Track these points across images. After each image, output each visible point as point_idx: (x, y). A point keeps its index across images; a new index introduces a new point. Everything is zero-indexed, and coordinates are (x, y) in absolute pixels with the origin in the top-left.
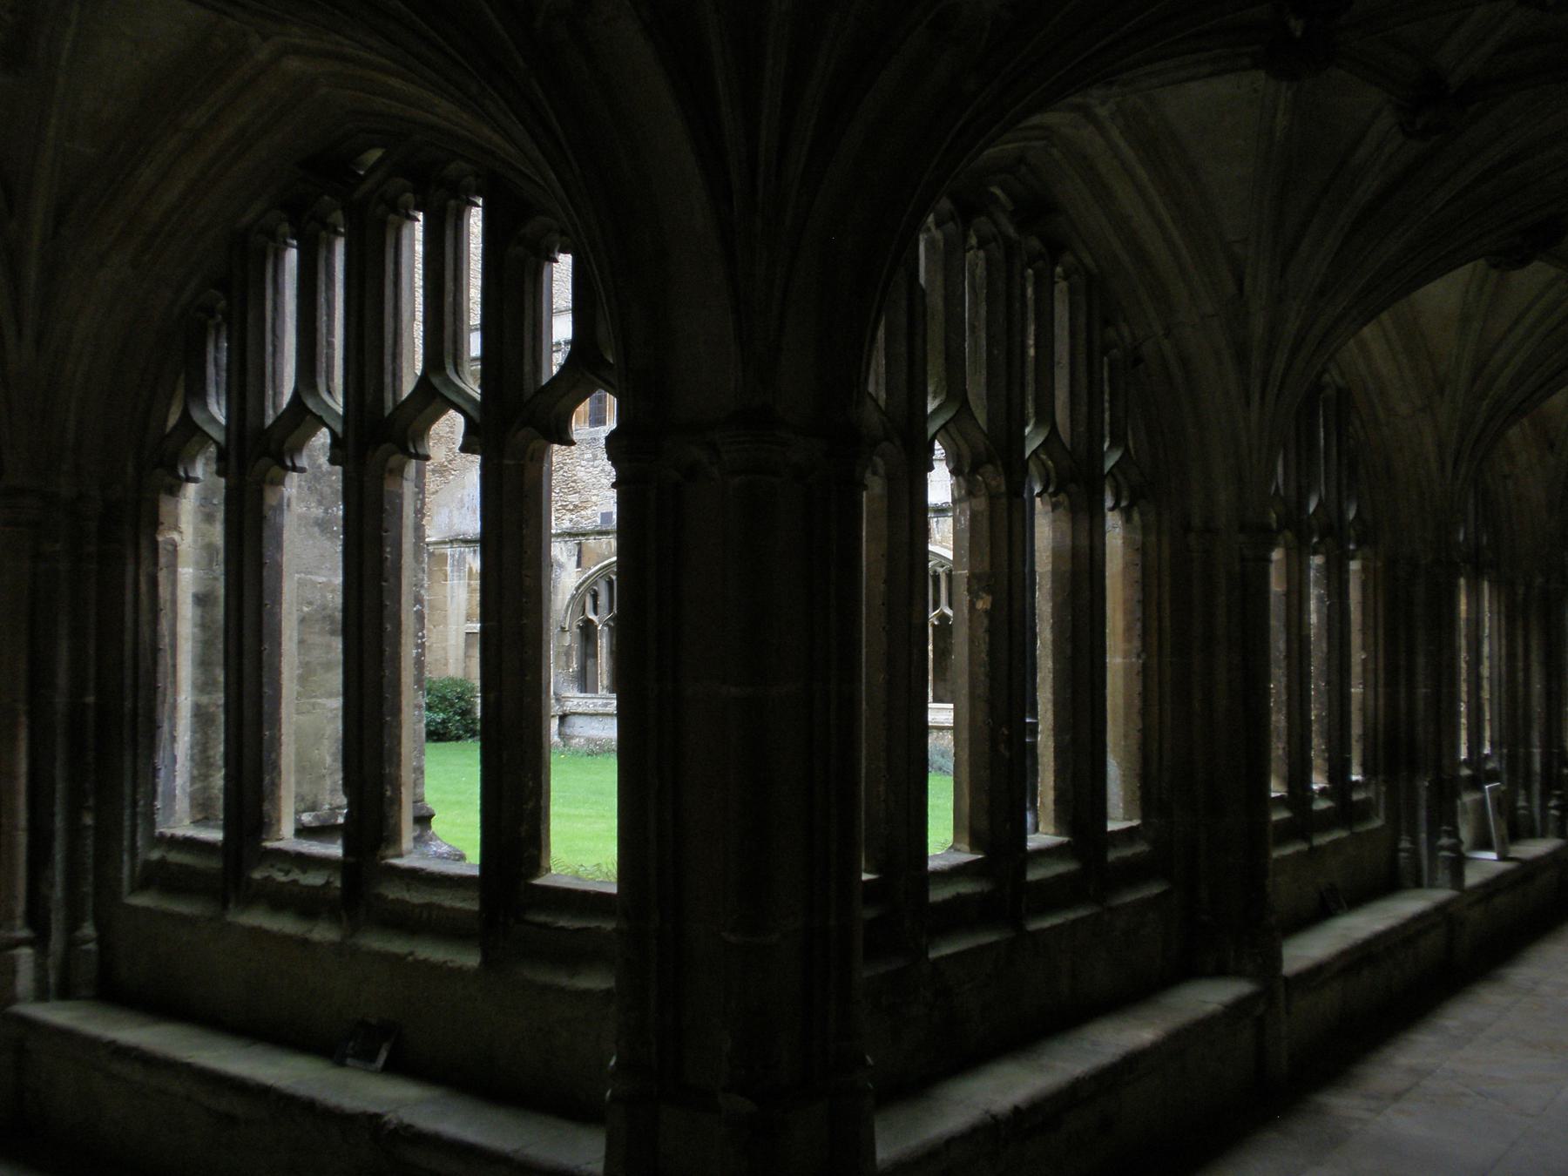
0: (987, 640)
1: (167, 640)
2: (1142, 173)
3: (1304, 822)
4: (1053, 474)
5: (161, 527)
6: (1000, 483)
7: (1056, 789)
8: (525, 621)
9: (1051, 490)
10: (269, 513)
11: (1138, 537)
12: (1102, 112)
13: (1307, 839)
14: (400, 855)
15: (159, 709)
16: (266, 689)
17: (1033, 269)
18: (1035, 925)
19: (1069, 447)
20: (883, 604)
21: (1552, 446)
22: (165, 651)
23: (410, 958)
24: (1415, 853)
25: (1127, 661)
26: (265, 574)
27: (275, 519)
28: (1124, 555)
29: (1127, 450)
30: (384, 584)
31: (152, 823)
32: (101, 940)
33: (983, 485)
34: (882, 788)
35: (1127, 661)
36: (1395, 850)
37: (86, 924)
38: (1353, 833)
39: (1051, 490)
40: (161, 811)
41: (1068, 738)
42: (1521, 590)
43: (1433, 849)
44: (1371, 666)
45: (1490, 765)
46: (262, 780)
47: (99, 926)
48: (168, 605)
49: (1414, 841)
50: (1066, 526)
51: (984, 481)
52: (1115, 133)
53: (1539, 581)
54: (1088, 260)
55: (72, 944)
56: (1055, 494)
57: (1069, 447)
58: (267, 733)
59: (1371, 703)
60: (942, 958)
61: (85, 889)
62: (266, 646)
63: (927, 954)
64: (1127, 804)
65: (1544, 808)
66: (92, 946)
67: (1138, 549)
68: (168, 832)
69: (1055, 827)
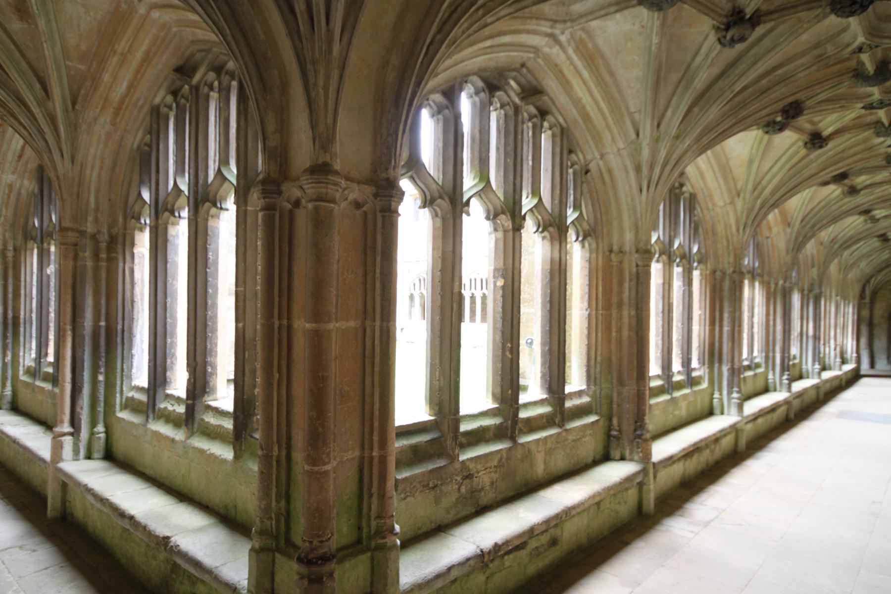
0: (501, 300)
1: (139, 297)
2: (585, 74)
3: (670, 386)
6: (509, 224)
10: (170, 238)
11: (588, 255)
12: (563, 38)
13: (671, 394)
14: (216, 400)
15: (135, 328)
16: (168, 320)
19: (550, 210)
21: (789, 225)
22: (138, 302)
24: (721, 400)
25: (582, 312)
29: (581, 214)
30: (208, 270)
31: (130, 378)
32: (107, 432)
33: (501, 225)
36: (712, 399)
37: (99, 425)
38: (692, 391)
39: (540, 230)
41: (547, 348)
42: (773, 286)
43: (730, 398)
44: (703, 317)
45: (757, 360)
47: (106, 426)
48: (140, 281)
49: (721, 394)
53: (781, 282)
54: (561, 120)
55: (92, 434)
56: (542, 232)
57: (550, 210)
59: (702, 333)
61: (99, 409)
63: (458, 458)
65: (781, 380)
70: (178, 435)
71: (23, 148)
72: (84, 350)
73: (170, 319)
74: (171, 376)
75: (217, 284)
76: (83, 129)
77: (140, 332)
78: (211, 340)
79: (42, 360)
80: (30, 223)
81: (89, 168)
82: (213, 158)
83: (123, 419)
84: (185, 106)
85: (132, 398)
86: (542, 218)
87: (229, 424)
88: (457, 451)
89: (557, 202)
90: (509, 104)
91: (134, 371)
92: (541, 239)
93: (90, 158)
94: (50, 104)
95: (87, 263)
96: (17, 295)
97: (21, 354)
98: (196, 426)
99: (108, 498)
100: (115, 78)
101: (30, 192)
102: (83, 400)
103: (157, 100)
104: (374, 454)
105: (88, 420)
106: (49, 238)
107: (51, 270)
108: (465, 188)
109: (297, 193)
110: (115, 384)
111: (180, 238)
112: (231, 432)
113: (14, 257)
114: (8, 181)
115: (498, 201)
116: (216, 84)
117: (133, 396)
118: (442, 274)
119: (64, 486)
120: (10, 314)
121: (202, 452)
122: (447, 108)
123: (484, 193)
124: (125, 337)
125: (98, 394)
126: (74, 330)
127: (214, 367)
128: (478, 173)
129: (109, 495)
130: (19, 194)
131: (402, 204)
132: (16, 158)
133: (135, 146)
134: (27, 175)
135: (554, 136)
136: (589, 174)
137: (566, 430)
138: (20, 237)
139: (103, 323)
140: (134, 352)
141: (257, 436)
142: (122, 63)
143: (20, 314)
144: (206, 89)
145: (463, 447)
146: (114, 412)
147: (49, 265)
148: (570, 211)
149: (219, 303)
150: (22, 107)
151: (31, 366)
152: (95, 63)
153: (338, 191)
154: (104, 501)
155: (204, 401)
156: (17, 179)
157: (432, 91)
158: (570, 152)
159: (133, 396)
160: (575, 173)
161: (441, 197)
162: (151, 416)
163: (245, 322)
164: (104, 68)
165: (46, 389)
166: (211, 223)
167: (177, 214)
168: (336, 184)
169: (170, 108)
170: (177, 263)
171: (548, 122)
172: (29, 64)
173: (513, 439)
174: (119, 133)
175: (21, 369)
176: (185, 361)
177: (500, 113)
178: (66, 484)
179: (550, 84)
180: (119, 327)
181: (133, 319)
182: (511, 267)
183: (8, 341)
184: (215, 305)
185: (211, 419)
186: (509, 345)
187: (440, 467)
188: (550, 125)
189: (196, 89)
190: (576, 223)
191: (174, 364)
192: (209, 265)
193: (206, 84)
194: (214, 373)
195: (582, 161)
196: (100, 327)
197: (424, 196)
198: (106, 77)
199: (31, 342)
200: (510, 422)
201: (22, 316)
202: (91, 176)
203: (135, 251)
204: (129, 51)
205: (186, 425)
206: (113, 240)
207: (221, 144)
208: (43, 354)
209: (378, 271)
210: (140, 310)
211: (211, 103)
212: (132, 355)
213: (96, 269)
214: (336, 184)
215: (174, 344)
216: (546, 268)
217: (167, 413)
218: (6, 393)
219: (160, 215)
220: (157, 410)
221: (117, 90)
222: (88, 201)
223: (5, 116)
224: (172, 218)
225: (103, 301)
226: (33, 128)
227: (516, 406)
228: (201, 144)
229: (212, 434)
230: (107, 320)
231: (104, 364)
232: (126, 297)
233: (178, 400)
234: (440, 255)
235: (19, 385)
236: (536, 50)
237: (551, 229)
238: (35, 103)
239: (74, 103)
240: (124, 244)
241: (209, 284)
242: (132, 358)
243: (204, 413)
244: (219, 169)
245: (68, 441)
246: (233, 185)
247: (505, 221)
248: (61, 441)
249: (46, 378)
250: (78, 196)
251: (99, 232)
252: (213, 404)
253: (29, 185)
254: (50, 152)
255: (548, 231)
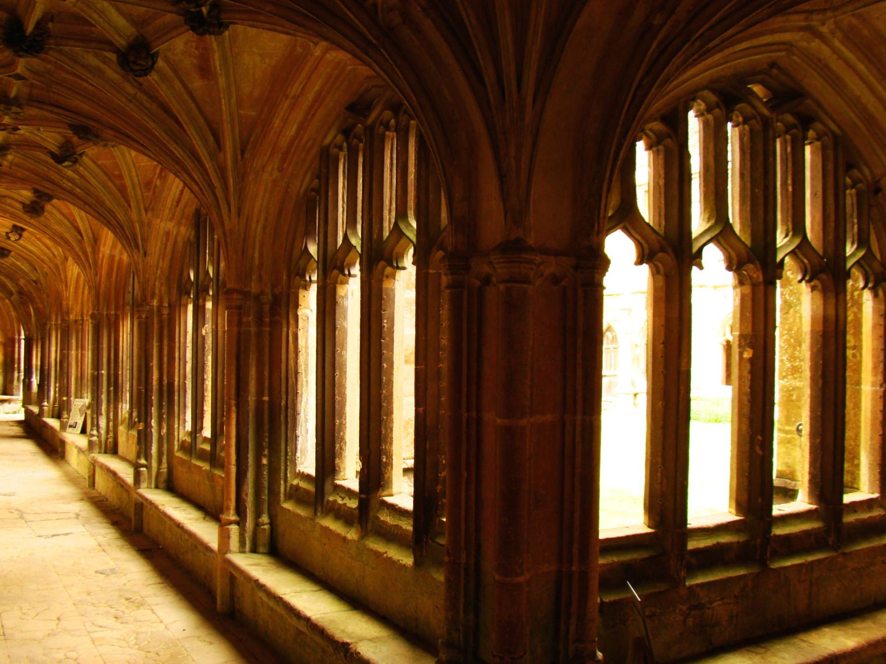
1: (303, 367)
2: (861, 67)
4: (808, 266)
5: (300, 307)
6: (759, 276)
7: (810, 473)
8: (441, 365)
9: (807, 278)
10: (339, 300)
12: (824, 29)
14: (391, 495)
15: (299, 405)
16: (337, 397)
17: (790, 135)
18: (776, 565)
20: (662, 357)
22: (302, 373)
23: (385, 555)
25: (874, 388)
26: (337, 333)
27: (343, 303)
28: (873, 319)
29: (869, 254)
30: (382, 341)
31: (294, 464)
32: (272, 523)
33: (748, 278)
34: (659, 474)
35: (874, 388)
37: (264, 515)
39: (807, 278)
40: (299, 459)
41: (818, 441)
46: (334, 447)
47: (271, 517)
50: (819, 302)
51: (748, 274)
52: (837, 43)
54: (833, 126)
55: (257, 525)
58: (337, 421)
60: (697, 585)
62: (337, 373)
63: (685, 582)
64: (871, 483)
66: (266, 527)
67: (882, 315)
68: (302, 470)
69: (809, 498)
70: (352, 535)
71: (182, 192)
72: (248, 429)
73: (339, 397)
74: (340, 464)
75: (392, 356)
76: (250, 178)
77: (304, 409)
78: (386, 425)
79: (198, 435)
80: (185, 274)
81: (255, 220)
82: (388, 208)
83: (289, 510)
84: (358, 146)
85: (297, 487)
86: (810, 262)
87: (407, 526)
88: (683, 574)
89: (831, 237)
90: (754, 117)
91: (298, 454)
92: (809, 290)
93: (256, 210)
94: (221, 156)
95: (251, 328)
96: (171, 358)
97: (176, 426)
98: (369, 524)
99: (281, 596)
100: (285, 122)
101: (186, 239)
102: (248, 485)
103: (328, 140)
104: (574, 568)
105: (253, 509)
106: (204, 293)
107: (207, 330)
108: (695, 234)
109: (487, 269)
110: (280, 469)
111: (349, 299)
112: (411, 535)
113: (169, 314)
114: (166, 229)
115: (741, 247)
116: (393, 122)
117: (298, 484)
118: (665, 347)
119: (232, 578)
120: (165, 382)
121: (378, 555)
122: (669, 136)
123: (723, 238)
124: (289, 415)
125: (262, 480)
126: (238, 406)
127: (390, 457)
128: (715, 212)
129: (282, 593)
130: (175, 242)
131: (607, 273)
132: (175, 203)
133: (302, 191)
134: (183, 221)
135: (824, 148)
136: (880, 195)
137: (844, 554)
138: (175, 292)
139: (266, 398)
140: (298, 432)
141: (442, 541)
142: (293, 107)
143: (174, 381)
144: (382, 129)
145: (692, 570)
146: (279, 502)
147: (204, 324)
148: (849, 249)
149: (394, 380)
150: (196, 162)
151: (185, 440)
152: (266, 109)
153: (532, 269)
154: (278, 599)
155: (378, 496)
156: (174, 226)
157: (652, 119)
158: (849, 167)
159: (298, 484)
160: (859, 194)
161: (663, 250)
162: (319, 509)
163: (426, 407)
164: (275, 113)
165: (204, 468)
166: (386, 285)
167: (347, 272)
168: (530, 262)
169: (341, 149)
170: (346, 329)
171: (814, 130)
172: (206, 119)
173: (763, 564)
174: (286, 180)
175: (176, 443)
176: (357, 449)
177: (744, 129)
178: (235, 575)
179: (814, 83)
180: (283, 403)
181: (297, 393)
182: (762, 333)
183: (164, 411)
184: (390, 382)
185: (386, 517)
186: (760, 438)
187: (660, 593)
188: (817, 134)
189: (370, 130)
190: (863, 263)
191: (343, 450)
192: (383, 335)
193: (381, 124)
194: (390, 464)
195: (869, 178)
196: (263, 401)
197: (640, 249)
198: (277, 122)
199: (185, 413)
200: (759, 541)
201: (176, 383)
202: (256, 230)
203: (299, 313)
204: (301, 92)
205: (360, 523)
206: (276, 302)
207: (399, 193)
208: (198, 427)
209: (579, 356)
210: (304, 383)
211: (386, 144)
212: (296, 436)
213: (259, 334)
214: (530, 262)
215: (343, 426)
216: (818, 329)
217: (336, 507)
218: (161, 471)
219: (329, 274)
220: (325, 503)
221: (287, 134)
222: (253, 257)
223: (179, 172)
224: (341, 277)
225: (266, 373)
226: (204, 183)
227: (768, 519)
228: (375, 193)
229: (390, 536)
230: (270, 395)
231: (267, 445)
232: (289, 367)
233: (349, 492)
234: (663, 323)
235: (175, 462)
236: (788, 46)
237: (823, 276)
238: (208, 157)
239: (243, 152)
240: (288, 306)
241: (383, 357)
242: (296, 440)
243: (378, 511)
244: (396, 224)
245: (234, 529)
246: (412, 242)
247: (754, 272)
248: (228, 529)
249: (202, 455)
250: (243, 252)
251: (262, 292)
252: (389, 499)
253: (185, 232)
254: (219, 206)
255: (818, 279)
